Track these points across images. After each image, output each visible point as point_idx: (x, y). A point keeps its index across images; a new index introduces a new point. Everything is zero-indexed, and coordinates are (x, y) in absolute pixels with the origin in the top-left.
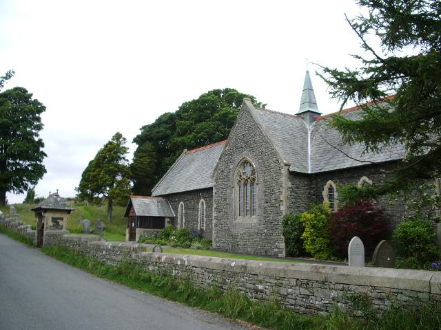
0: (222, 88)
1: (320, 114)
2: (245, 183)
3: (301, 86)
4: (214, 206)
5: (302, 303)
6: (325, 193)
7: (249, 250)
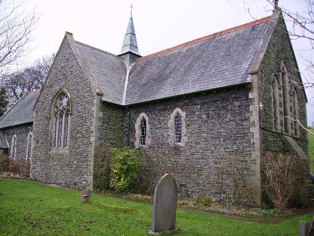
6: (137, 125)
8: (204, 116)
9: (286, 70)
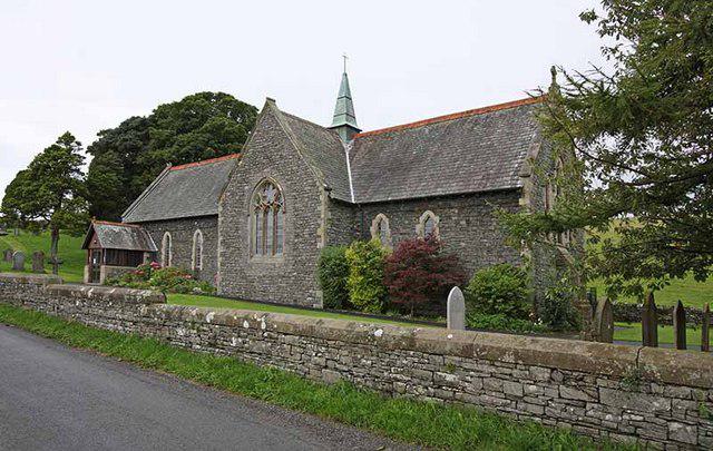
0: (215, 91)
3: (336, 92)
4: (221, 239)
5: (564, 415)
8: (463, 222)
9: (561, 166)
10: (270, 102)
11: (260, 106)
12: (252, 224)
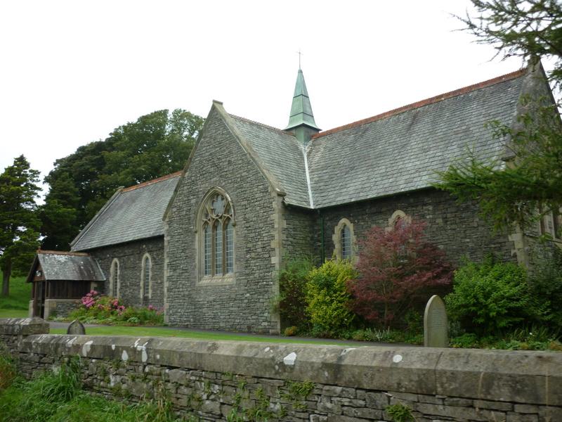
1: (319, 130)
2: (214, 225)
4: (167, 261)
6: (336, 238)
7: (222, 325)
8: (440, 221)
10: (216, 109)
11: (203, 113)
12: (200, 241)
